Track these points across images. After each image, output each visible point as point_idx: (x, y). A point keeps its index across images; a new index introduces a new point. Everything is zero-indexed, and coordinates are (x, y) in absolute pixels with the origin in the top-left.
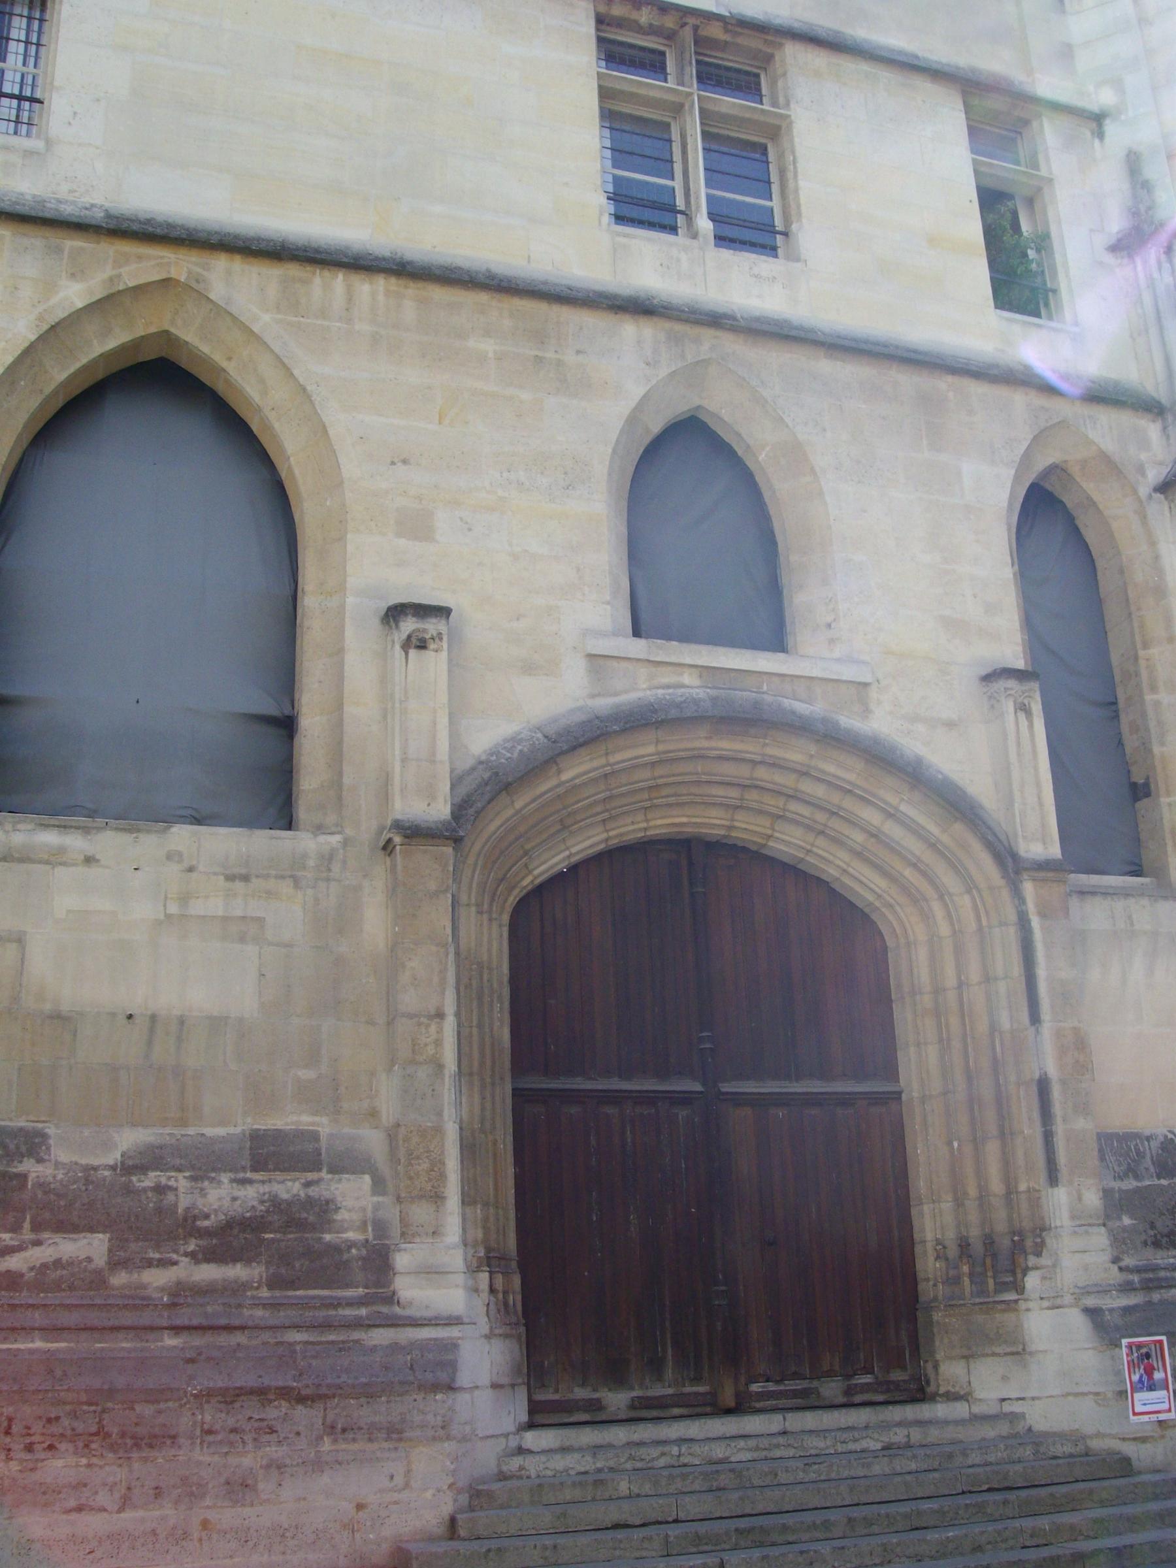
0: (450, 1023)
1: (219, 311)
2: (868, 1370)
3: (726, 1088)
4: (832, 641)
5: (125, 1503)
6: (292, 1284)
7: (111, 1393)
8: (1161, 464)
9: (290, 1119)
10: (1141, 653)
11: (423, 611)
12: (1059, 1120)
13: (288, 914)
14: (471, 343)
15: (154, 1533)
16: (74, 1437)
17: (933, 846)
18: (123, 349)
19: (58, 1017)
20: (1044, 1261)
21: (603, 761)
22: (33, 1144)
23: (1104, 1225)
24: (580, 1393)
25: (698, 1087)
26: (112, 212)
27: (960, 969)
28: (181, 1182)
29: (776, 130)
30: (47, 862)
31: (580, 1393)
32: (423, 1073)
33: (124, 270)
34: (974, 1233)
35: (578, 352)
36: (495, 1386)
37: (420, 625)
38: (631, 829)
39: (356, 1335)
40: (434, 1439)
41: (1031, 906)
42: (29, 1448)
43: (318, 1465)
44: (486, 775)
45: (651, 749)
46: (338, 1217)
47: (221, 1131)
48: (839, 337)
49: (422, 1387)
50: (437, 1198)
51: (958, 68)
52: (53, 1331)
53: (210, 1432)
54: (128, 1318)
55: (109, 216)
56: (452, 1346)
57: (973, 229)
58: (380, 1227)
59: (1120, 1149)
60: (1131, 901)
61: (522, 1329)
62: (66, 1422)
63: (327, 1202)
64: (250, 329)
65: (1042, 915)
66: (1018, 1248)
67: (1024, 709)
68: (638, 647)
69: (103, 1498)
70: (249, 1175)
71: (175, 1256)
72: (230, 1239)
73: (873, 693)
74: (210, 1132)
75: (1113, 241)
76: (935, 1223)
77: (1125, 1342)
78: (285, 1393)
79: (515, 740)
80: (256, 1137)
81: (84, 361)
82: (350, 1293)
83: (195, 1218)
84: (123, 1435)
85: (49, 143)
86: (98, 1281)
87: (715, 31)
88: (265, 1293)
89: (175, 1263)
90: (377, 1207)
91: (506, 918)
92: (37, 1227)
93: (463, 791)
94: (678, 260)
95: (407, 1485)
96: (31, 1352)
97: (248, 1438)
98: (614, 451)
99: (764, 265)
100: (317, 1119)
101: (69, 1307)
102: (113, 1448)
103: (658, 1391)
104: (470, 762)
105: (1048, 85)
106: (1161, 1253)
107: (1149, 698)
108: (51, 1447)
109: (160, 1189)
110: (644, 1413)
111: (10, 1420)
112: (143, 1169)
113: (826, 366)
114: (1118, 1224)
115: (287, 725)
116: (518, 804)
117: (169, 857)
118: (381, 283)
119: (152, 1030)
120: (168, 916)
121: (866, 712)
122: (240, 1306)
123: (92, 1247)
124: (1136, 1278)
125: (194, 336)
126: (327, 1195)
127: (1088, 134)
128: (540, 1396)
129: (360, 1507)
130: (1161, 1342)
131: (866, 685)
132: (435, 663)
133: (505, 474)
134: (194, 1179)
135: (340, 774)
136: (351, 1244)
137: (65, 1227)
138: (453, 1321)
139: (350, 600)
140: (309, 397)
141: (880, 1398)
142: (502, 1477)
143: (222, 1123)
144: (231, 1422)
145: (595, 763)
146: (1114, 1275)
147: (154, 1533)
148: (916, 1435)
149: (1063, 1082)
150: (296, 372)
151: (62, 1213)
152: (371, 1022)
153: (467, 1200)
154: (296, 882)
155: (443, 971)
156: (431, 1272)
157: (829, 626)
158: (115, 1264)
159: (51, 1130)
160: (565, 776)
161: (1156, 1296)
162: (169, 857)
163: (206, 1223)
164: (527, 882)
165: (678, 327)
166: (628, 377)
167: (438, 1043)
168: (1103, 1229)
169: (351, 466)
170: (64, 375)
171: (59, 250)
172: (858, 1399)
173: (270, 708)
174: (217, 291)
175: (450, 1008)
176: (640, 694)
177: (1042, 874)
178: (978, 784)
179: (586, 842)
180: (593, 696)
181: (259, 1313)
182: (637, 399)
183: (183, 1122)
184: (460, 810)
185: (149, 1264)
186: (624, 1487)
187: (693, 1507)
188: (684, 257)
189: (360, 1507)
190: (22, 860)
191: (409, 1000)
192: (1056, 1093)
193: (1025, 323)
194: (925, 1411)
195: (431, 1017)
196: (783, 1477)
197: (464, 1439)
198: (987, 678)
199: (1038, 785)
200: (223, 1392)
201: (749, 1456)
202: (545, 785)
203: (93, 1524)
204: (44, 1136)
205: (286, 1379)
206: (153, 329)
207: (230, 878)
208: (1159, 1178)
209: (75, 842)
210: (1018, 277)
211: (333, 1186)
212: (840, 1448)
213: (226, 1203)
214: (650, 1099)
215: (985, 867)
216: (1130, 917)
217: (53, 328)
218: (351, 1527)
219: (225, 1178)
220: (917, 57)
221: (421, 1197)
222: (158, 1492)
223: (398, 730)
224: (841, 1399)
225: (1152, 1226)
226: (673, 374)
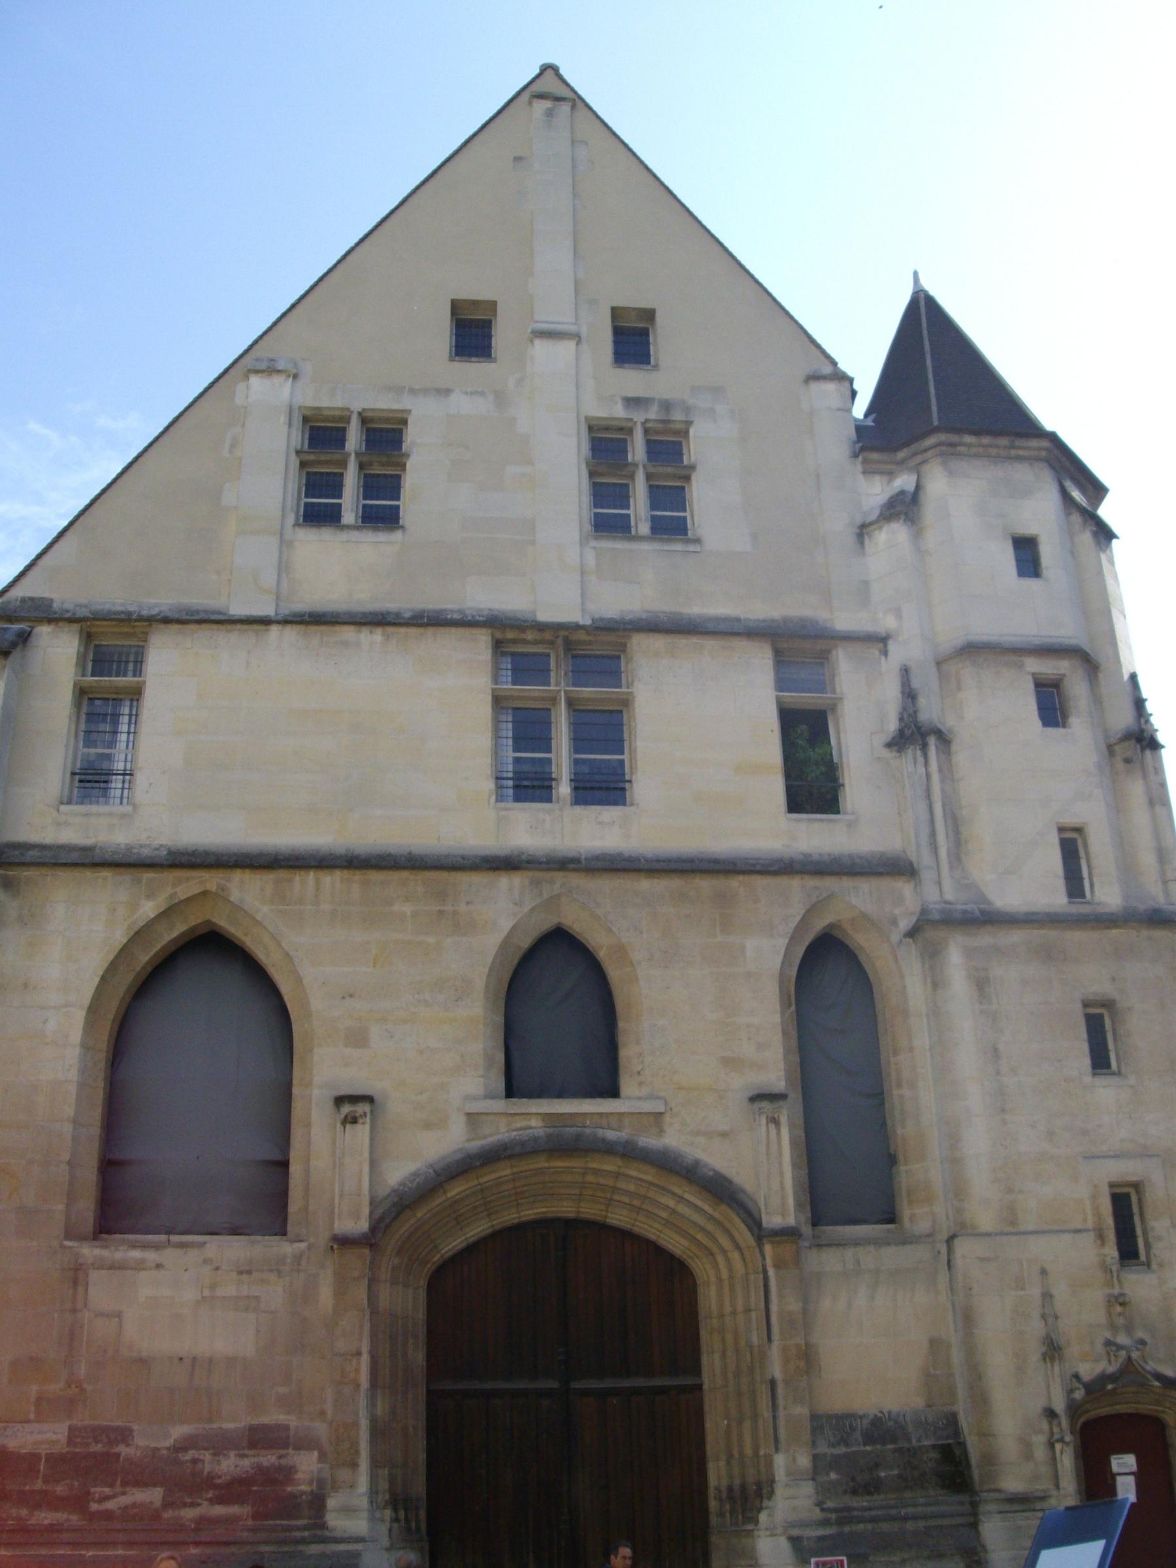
0: (365, 1358)
1: (237, 908)
4: (641, 1084)
6: (267, 1516)
11: (354, 1099)
12: (781, 1408)
13: (274, 1293)
14: (396, 908)
17: (711, 1218)
18: (183, 934)
21: (476, 1182)
22: (124, 1435)
23: (813, 1479)
25: (553, 1384)
28: (207, 1456)
29: (627, 702)
30: (135, 1269)
33: (179, 889)
35: (468, 903)
37: (352, 1109)
39: (300, 1548)
41: (769, 1262)
45: (508, 1172)
46: (297, 1477)
48: (658, 861)
50: (354, 1465)
51: (773, 621)
52: (129, 1544)
56: (357, 1555)
59: (833, 1426)
64: (255, 910)
65: (777, 1266)
67: (775, 1121)
68: (500, 1105)
70: (246, 1452)
71: (199, 1501)
72: (232, 1490)
73: (667, 1118)
77: (813, 1560)
79: (415, 1174)
80: (252, 1429)
82: (300, 1523)
83: (213, 1478)
85: (135, 806)
86: (156, 1516)
87: (581, 636)
88: (250, 1522)
89: (199, 1505)
90: (320, 1471)
96: (117, 1556)
98: (490, 970)
99: (610, 813)
100: (289, 1417)
104: (387, 1191)
107: (895, 1092)
109: (195, 1461)
112: (185, 1449)
113: (645, 884)
114: (825, 1478)
116: (419, 1215)
117: (205, 1261)
118: (338, 874)
121: (661, 1131)
123: (154, 1496)
130: (842, 1561)
131: (661, 1114)
133: (417, 996)
136: (303, 1493)
137: (140, 1483)
138: (359, 1540)
140: (291, 959)
146: (817, 1514)
150: (283, 944)
153: (375, 1464)
154: (279, 1272)
155: (361, 1327)
156: (348, 1511)
157: (639, 1073)
158: (167, 1505)
159: (135, 1427)
160: (449, 1195)
161: (847, 1529)
162: (205, 1261)
165: (539, 875)
166: (503, 914)
167: (357, 1371)
169: (317, 1003)
171: (139, 881)
174: (235, 895)
175: (365, 1349)
176: (500, 1137)
178: (742, 1175)
181: (245, 1534)
184: (373, 1229)
185: (185, 1505)
192: (780, 1390)
193: (809, 820)
202: (438, 1201)
204: (131, 1431)
206: (199, 921)
207: (240, 1273)
208: (865, 1444)
209: (151, 1256)
210: (812, 784)
213: (232, 1468)
215: (745, 1236)
217: (137, 933)
219: (232, 1454)
220: (738, 620)
223: (340, 1176)
225: (853, 1479)
226: (533, 909)
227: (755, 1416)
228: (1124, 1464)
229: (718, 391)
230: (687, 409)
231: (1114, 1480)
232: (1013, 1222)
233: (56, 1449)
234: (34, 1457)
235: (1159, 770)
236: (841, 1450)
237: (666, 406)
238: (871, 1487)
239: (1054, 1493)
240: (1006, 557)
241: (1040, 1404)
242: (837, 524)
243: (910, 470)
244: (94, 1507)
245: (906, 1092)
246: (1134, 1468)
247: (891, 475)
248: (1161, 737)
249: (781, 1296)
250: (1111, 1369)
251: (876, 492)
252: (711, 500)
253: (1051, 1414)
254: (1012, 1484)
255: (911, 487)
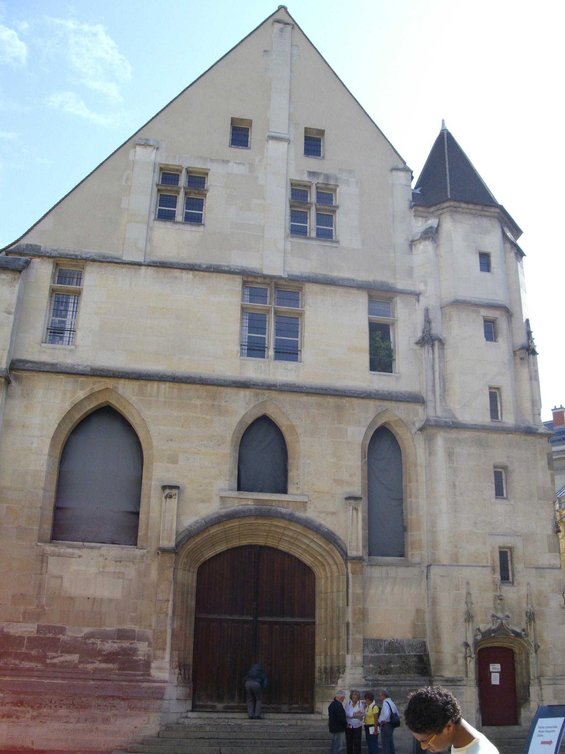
0: (171, 603)
1: (121, 396)
2: (297, 703)
3: (260, 619)
4: (298, 488)
5: (78, 722)
7: (76, 694)
8: (422, 421)
9: (128, 626)
10: (408, 485)
12: (351, 635)
13: (131, 571)
14: (193, 402)
15: (84, 729)
16: (67, 704)
19: (70, 598)
20: (343, 676)
21: (222, 527)
22: (62, 630)
24: (209, 703)
26: (93, 367)
27: (332, 588)
28: (99, 642)
31: (209, 703)
32: (162, 616)
34: (329, 666)
35: (226, 402)
36: (177, 699)
38: (236, 543)
39: (139, 684)
40: (156, 712)
41: (349, 571)
42: (56, 707)
43: (126, 716)
44: (187, 533)
47: (110, 629)
49: (154, 698)
50: (164, 649)
52: (64, 678)
53: (100, 706)
54: (82, 676)
55: (92, 369)
56: (164, 688)
57: (365, 343)
58: (149, 656)
60: (389, 567)
61: (192, 685)
62: (65, 701)
63: (136, 649)
66: (339, 672)
67: (356, 509)
68: (236, 494)
69: (72, 720)
72: (110, 657)
73: (308, 505)
74: (107, 629)
75: (417, 340)
76: (320, 662)
78: (119, 697)
79: (196, 522)
80: (119, 630)
81: (84, 412)
83: (101, 651)
84: (78, 705)
86: (76, 666)
88: (117, 672)
90: (148, 651)
91: (196, 570)
92: (62, 652)
93: (180, 538)
94: (261, 366)
95: (148, 723)
96: (58, 683)
97: (109, 708)
101: (68, 672)
102: (76, 708)
103: (232, 704)
104: (184, 529)
105: (401, 284)
106: (380, 676)
107: (409, 500)
108: (61, 707)
109: (93, 643)
110: (227, 710)
111: (51, 700)
112: (89, 638)
113: (305, 399)
115: (137, 514)
116: (197, 541)
117: (101, 555)
119: (94, 601)
120: (99, 572)
121: (306, 510)
122: (110, 674)
123: (75, 658)
124: (370, 683)
125: (114, 403)
126: (136, 647)
127: (414, 300)
128: (198, 703)
129: (136, 727)
132: (174, 502)
134: (102, 641)
135: (147, 532)
136: (141, 660)
137: (69, 652)
139: (153, 483)
141: (300, 712)
142: (178, 723)
143: (111, 627)
144: (105, 704)
145: (221, 528)
147: (84, 729)
148: (299, 722)
149: (354, 624)
151: (68, 649)
152: (151, 601)
154: (134, 563)
156: (160, 669)
158: (80, 662)
159: (67, 627)
160: (211, 532)
163: (104, 653)
164: (203, 560)
166: (241, 408)
167: (167, 608)
168: (361, 668)
169: (156, 442)
170: (79, 417)
172: (293, 711)
173: (133, 510)
174: (121, 391)
175: (171, 598)
177: (354, 561)
179: (221, 548)
180: (220, 509)
181: (115, 677)
182: (242, 415)
183: (101, 626)
184: (177, 546)
185: (89, 662)
186: (208, 729)
187: (222, 735)
188: (263, 365)
189: (136, 727)
190: (63, 556)
191: (160, 596)
192: (351, 627)
194: (312, 716)
195: (166, 601)
196: (253, 730)
197: (165, 713)
198: (348, 498)
199: (357, 533)
200: (104, 696)
201: (248, 724)
203: (70, 726)
204: (65, 629)
205: (120, 694)
206: (103, 401)
207: (116, 561)
209: (77, 552)
210: (381, 358)
211: (138, 645)
212: (275, 724)
213: (110, 648)
214: (238, 621)
215: (339, 558)
216: (387, 572)
218: (133, 732)
219: (110, 641)
221: (160, 649)
222: (86, 720)
223: (163, 521)
224: (287, 711)
225: (380, 668)
226: (254, 407)
227: (339, 638)
228: (495, 668)
229: (351, 172)
230: (336, 179)
231: (490, 674)
232: (456, 561)
233: (32, 635)
234: (21, 638)
235: (535, 364)
236: (375, 654)
237: (327, 177)
238: (387, 671)
239: (465, 678)
240: (476, 261)
241: (461, 640)
242: (401, 240)
243: (435, 217)
244: (48, 661)
245: (414, 500)
246: (500, 670)
247: (426, 218)
248: (537, 350)
249: (353, 586)
250: (494, 627)
251: (419, 226)
252: (344, 223)
253: (466, 645)
254: (448, 674)
255: (435, 225)
